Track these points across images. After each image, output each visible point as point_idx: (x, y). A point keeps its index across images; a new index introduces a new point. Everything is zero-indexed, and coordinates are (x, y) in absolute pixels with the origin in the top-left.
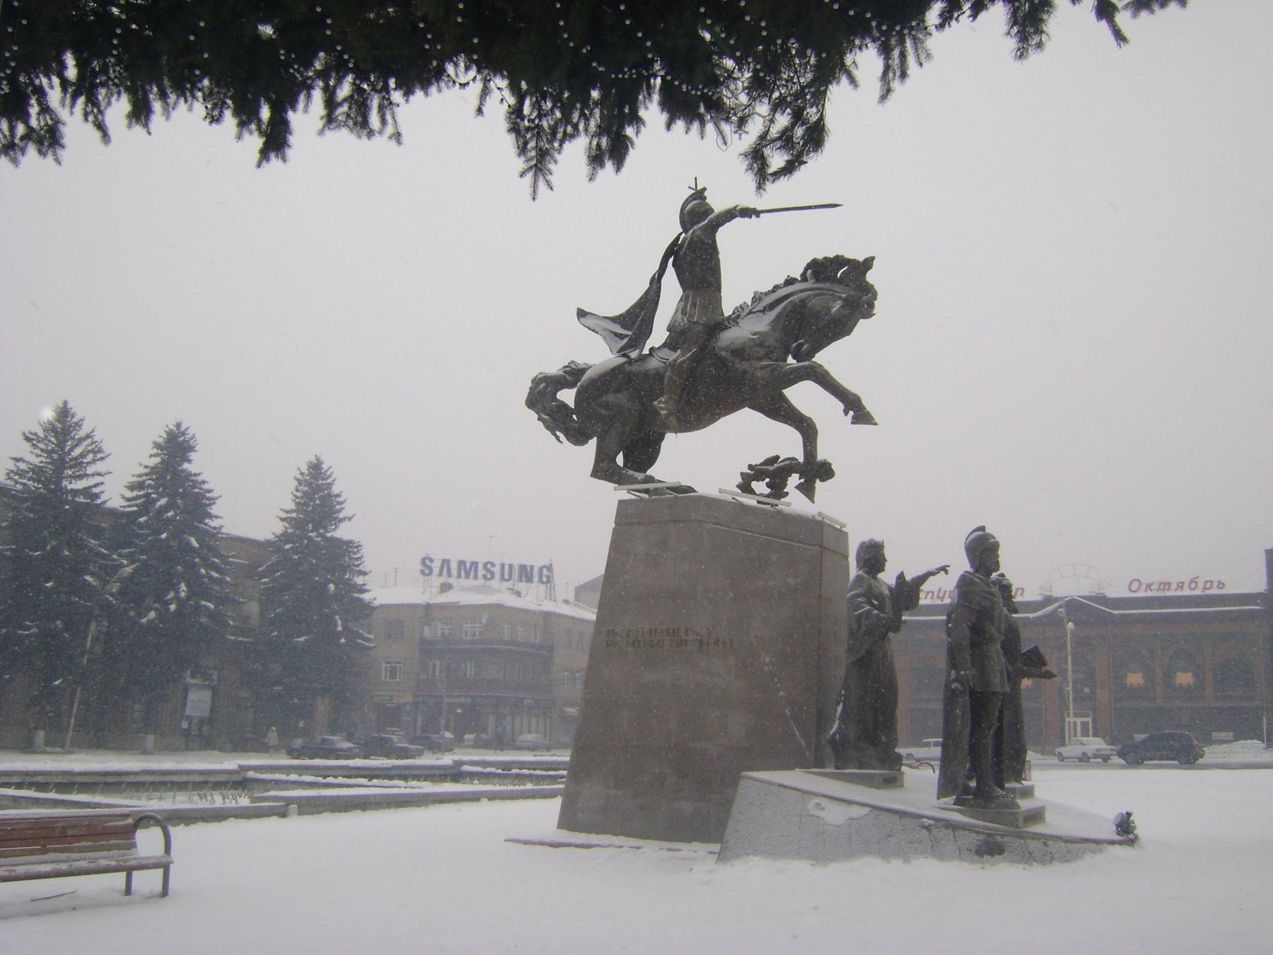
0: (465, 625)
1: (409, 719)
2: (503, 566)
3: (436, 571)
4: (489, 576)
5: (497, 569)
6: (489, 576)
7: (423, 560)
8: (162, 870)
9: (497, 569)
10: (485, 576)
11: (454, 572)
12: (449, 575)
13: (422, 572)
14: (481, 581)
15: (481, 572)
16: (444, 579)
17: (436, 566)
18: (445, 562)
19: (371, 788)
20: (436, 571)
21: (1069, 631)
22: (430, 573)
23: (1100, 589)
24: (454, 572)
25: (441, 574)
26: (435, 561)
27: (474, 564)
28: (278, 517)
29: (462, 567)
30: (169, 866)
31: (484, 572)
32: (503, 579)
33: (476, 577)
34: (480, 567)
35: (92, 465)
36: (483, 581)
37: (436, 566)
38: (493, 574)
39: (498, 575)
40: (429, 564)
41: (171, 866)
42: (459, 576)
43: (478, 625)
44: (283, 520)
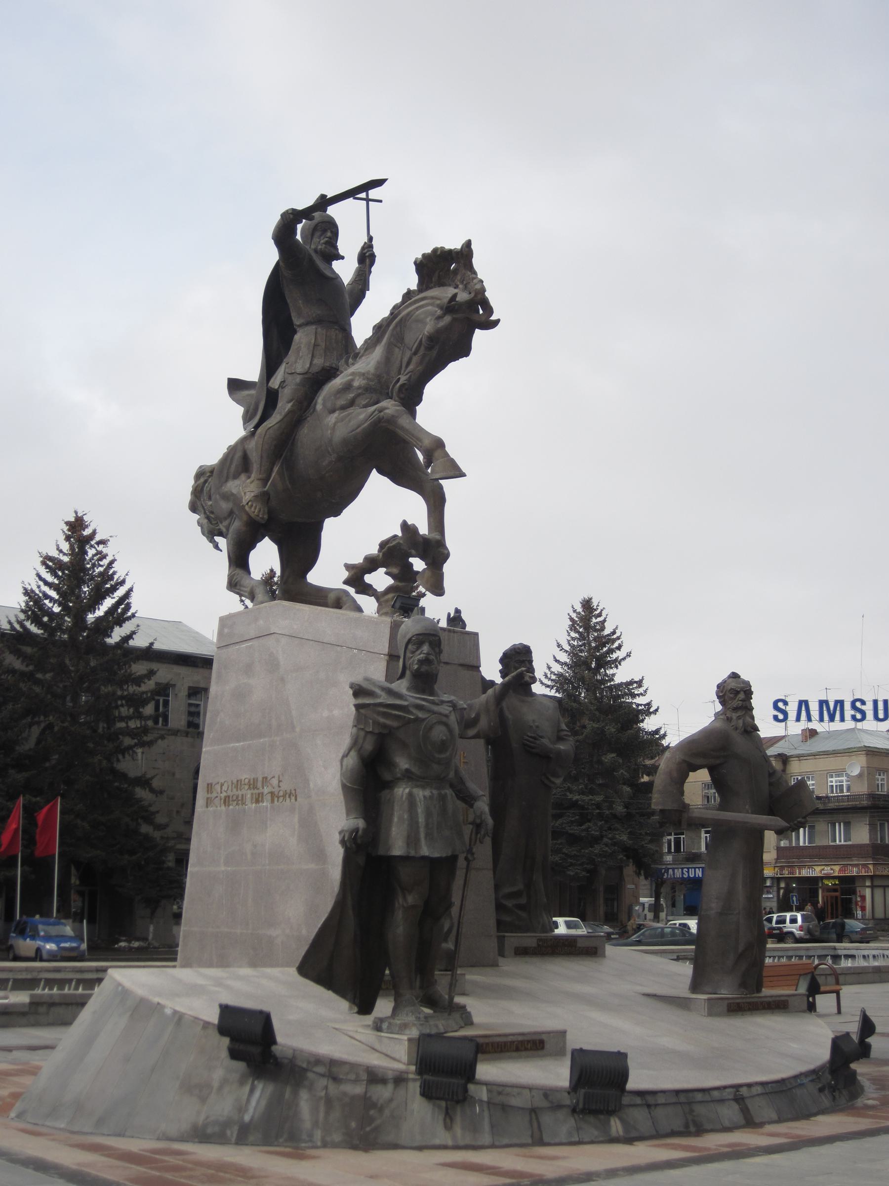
0: (830, 779)
1: (771, 896)
2: (875, 702)
3: (792, 715)
4: (859, 716)
5: (868, 708)
6: (859, 716)
7: (775, 704)
8: (835, 994)
9: (868, 708)
10: (854, 718)
11: (815, 714)
12: (809, 719)
13: (776, 718)
14: (849, 724)
15: (849, 712)
16: (803, 724)
17: (792, 709)
18: (803, 704)
19: (852, 950)
20: (792, 715)
21: (72, 912)
22: (786, 718)
23: (411, 350)
24: (815, 714)
25: (798, 719)
26: (789, 704)
27: (840, 703)
28: (7, 617)
29: (825, 708)
30: (839, 992)
31: (853, 712)
32: (876, 717)
33: (842, 719)
34: (847, 706)
35: (44, 567)
36: (853, 723)
37: (792, 709)
38: (785, 714)
39: (870, 714)
40: (783, 708)
41: (841, 991)
42: (821, 719)
43: (844, 778)
44: (10, 623)
